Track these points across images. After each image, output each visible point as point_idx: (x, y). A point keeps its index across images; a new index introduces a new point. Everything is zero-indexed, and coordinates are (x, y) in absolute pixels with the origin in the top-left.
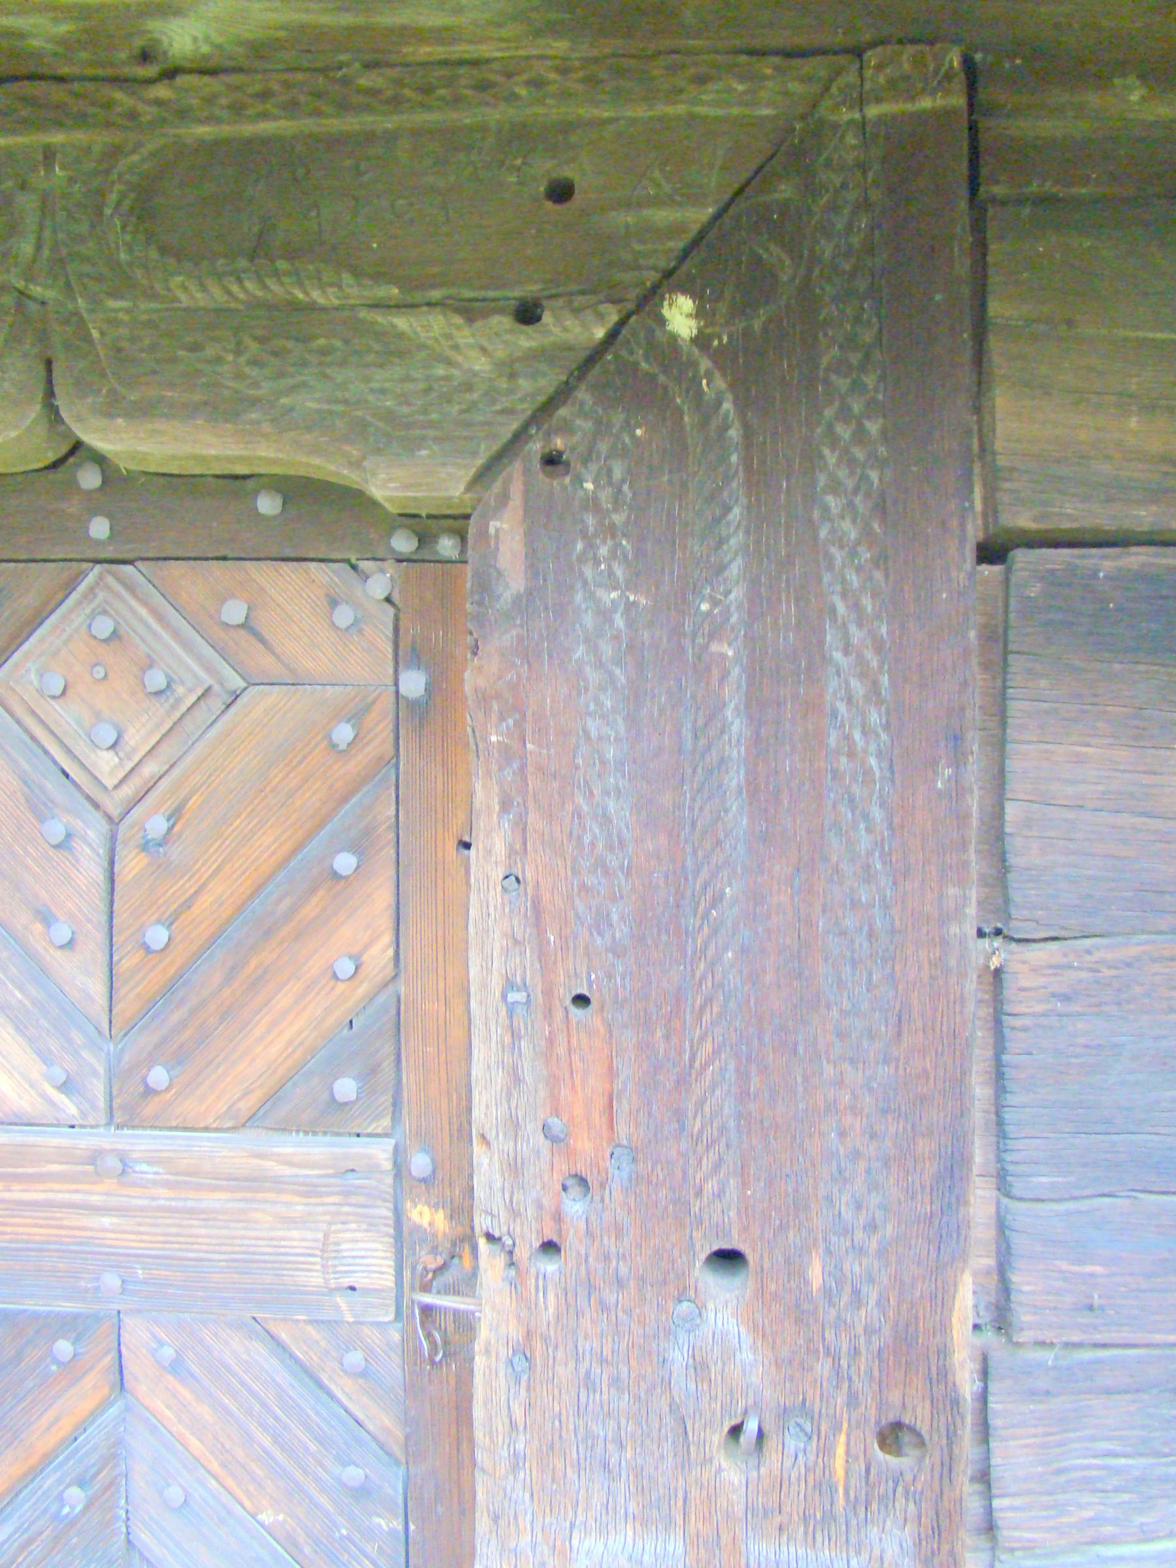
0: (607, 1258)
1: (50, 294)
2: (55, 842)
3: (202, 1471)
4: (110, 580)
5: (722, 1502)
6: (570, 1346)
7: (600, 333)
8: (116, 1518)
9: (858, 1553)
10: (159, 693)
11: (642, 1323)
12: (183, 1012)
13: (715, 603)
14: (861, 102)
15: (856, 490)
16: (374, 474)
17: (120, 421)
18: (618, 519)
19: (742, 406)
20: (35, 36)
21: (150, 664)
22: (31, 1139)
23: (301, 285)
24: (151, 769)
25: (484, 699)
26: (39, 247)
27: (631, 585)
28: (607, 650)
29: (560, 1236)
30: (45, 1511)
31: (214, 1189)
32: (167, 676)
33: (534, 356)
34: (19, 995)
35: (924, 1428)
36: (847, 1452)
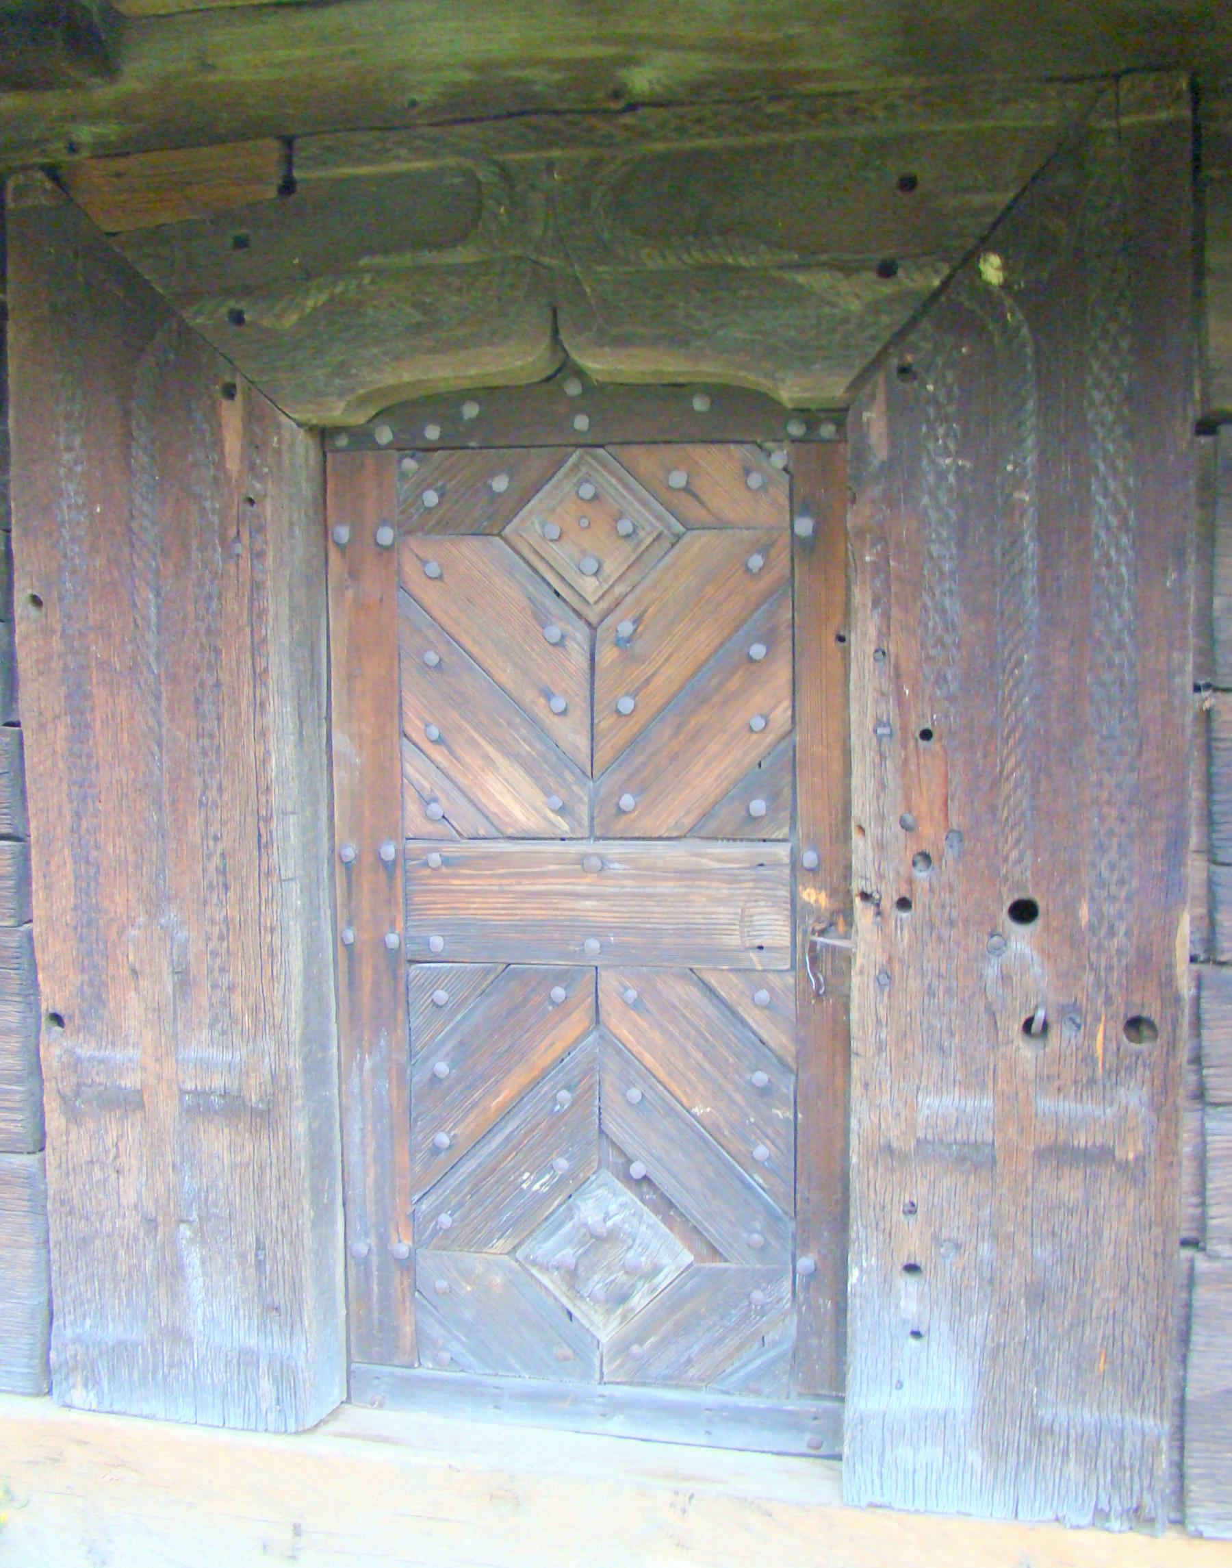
0: (943, 906)
1: (554, 263)
2: (553, 640)
4: (589, 459)
5: (1020, 1069)
6: (918, 966)
7: (936, 282)
8: (592, 1113)
10: (628, 536)
11: (966, 950)
12: (640, 760)
13: (1016, 465)
14: (1117, 114)
15: (1113, 386)
16: (783, 381)
18: (950, 409)
19: (1034, 331)
20: (535, 83)
21: (620, 516)
23: (731, 253)
24: (620, 589)
25: (861, 533)
26: (545, 230)
27: (959, 454)
28: (943, 498)
30: (543, 1108)
31: (664, 879)
33: (891, 300)
34: (528, 748)
35: (1157, 1021)
36: (1105, 1037)
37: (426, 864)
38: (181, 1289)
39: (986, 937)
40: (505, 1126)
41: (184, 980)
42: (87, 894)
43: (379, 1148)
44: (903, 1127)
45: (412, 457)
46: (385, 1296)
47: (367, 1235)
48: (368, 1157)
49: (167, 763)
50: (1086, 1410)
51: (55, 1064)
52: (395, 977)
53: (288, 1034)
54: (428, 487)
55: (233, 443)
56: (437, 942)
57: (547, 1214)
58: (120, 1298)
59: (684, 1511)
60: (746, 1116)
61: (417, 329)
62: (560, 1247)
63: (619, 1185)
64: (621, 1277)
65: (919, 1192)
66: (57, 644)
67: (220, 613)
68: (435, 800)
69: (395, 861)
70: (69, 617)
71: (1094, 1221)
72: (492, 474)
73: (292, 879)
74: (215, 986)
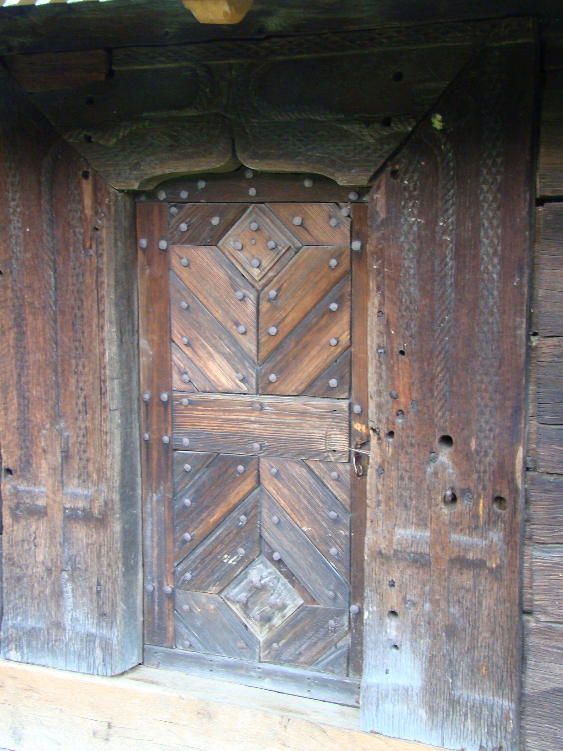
3: (285, 512)
4: (257, 209)
5: (442, 519)
7: (410, 129)
9: (486, 539)
10: (273, 249)
11: (419, 459)
12: (280, 357)
13: (444, 222)
17: (257, 160)
18: (416, 193)
22: (232, 398)
23: (313, 115)
24: (271, 274)
27: (419, 216)
29: (394, 428)
31: (291, 415)
32: (275, 243)
34: (228, 350)
37: (181, 404)
38: (62, 603)
39: (428, 453)
40: (216, 532)
41: (66, 457)
42: (24, 413)
43: (159, 539)
44: (387, 543)
45: (175, 206)
46: (161, 612)
47: (153, 581)
48: (154, 543)
49: (60, 353)
50: (476, 694)
51: (8, 493)
52: (168, 457)
53: (113, 482)
54: (182, 222)
55: (88, 201)
56: (186, 441)
57: (235, 575)
58: (34, 606)
59: (285, 727)
60: (327, 533)
61: (171, 148)
62: (240, 592)
63: (269, 563)
64: (267, 609)
65: (395, 576)
66: (9, 293)
67: (83, 283)
68: (186, 373)
69: (167, 402)
70: (15, 281)
71: (478, 597)
72: (212, 215)
73: (116, 410)
74: (81, 459)
